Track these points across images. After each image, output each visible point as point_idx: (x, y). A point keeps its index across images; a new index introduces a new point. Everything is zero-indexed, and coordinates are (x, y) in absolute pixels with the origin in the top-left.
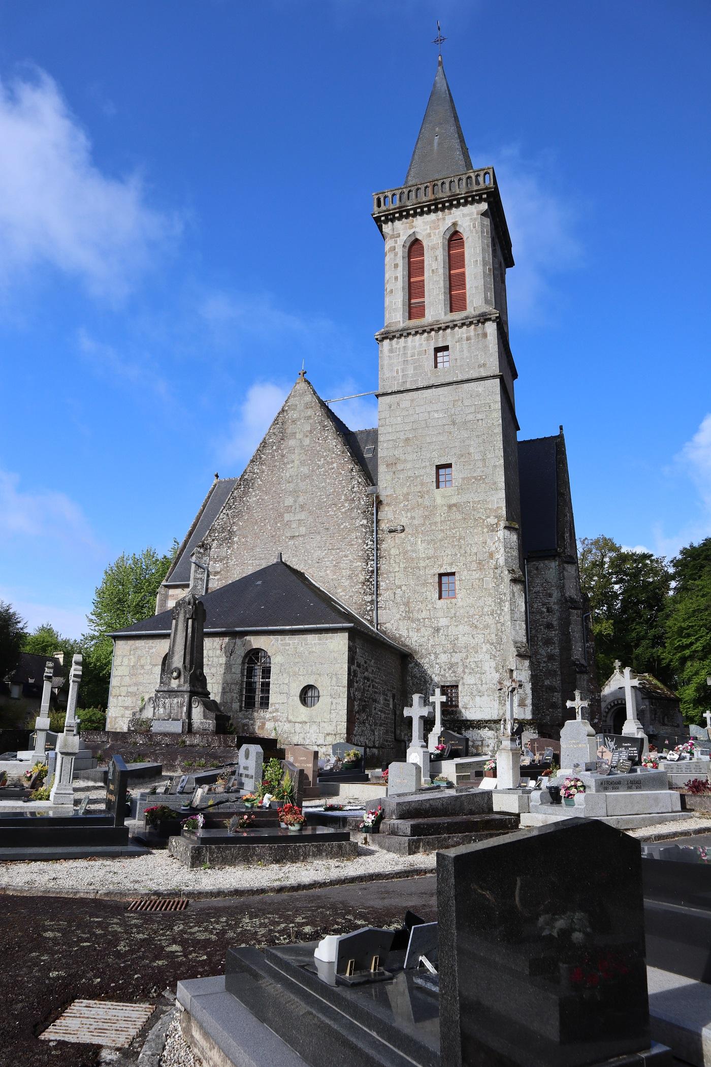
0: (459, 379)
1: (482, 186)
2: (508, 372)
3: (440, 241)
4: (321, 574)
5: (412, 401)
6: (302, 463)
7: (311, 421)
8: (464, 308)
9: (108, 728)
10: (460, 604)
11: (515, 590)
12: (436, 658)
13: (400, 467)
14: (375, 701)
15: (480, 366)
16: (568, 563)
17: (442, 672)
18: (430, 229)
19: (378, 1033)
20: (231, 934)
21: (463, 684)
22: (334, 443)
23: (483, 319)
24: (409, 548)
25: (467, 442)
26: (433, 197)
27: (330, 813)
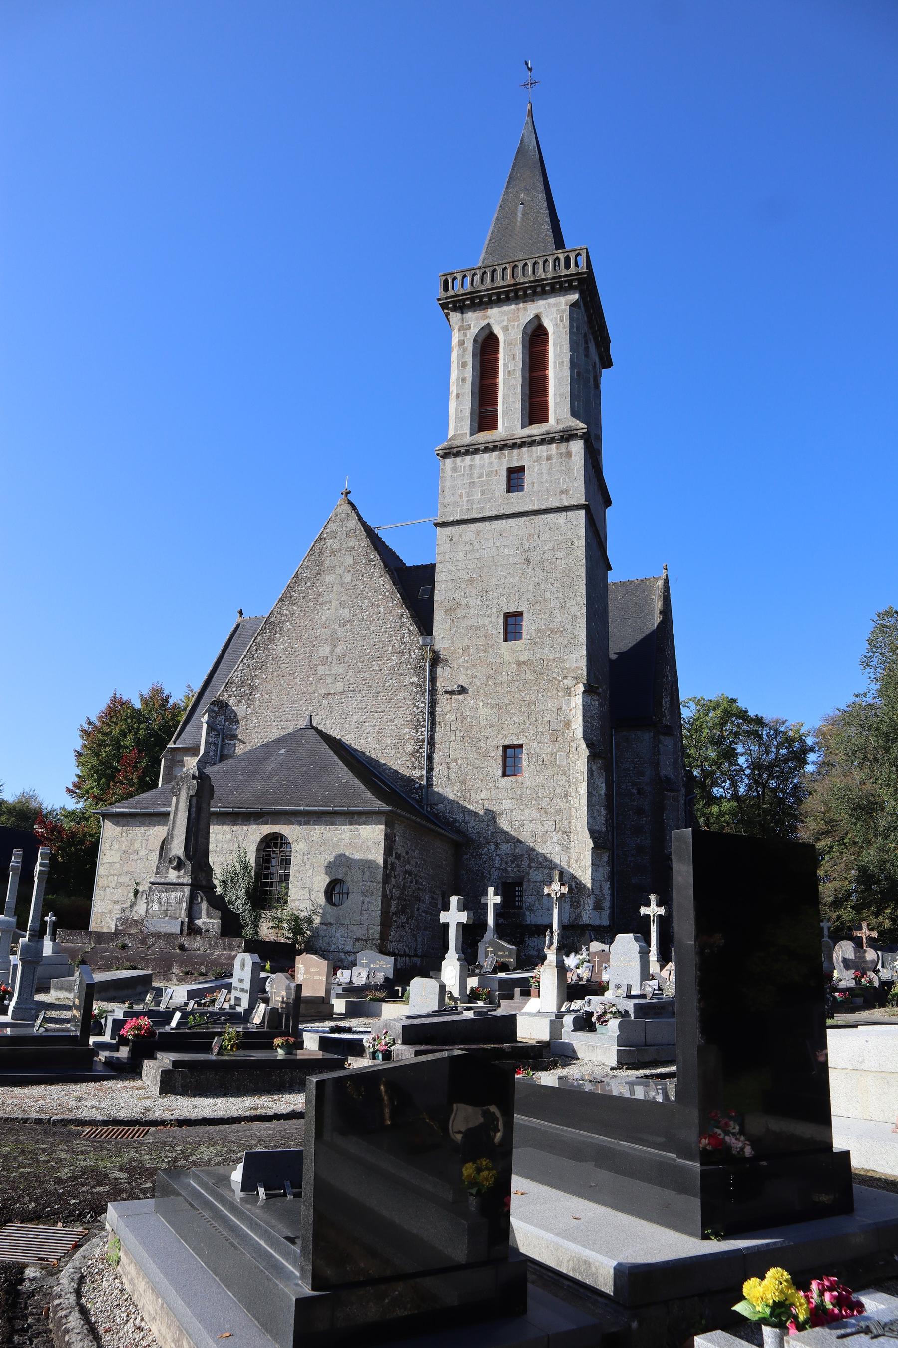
0: (536, 508)
1: (573, 269)
2: (598, 497)
3: (519, 336)
4: (362, 742)
5: (478, 532)
6: (342, 605)
7: (354, 553)
8: (545, 419)
9: (93, 926)
10: (528, 782)
11: (594, 768)
12: (497, 848)
13: (460, 613)
14: (419, 899)
15: (562, 493)
16: (665, 734)
17: (504, 866)
18: (508, 323)
19: (265, 1241)
20: (181, 1162)
21: (529, 881)
22: (382, 582)
23: (567, 436)
24: (468, 713)
25: (543, 586)
26: (512, 282)
27: (336, 1036)
